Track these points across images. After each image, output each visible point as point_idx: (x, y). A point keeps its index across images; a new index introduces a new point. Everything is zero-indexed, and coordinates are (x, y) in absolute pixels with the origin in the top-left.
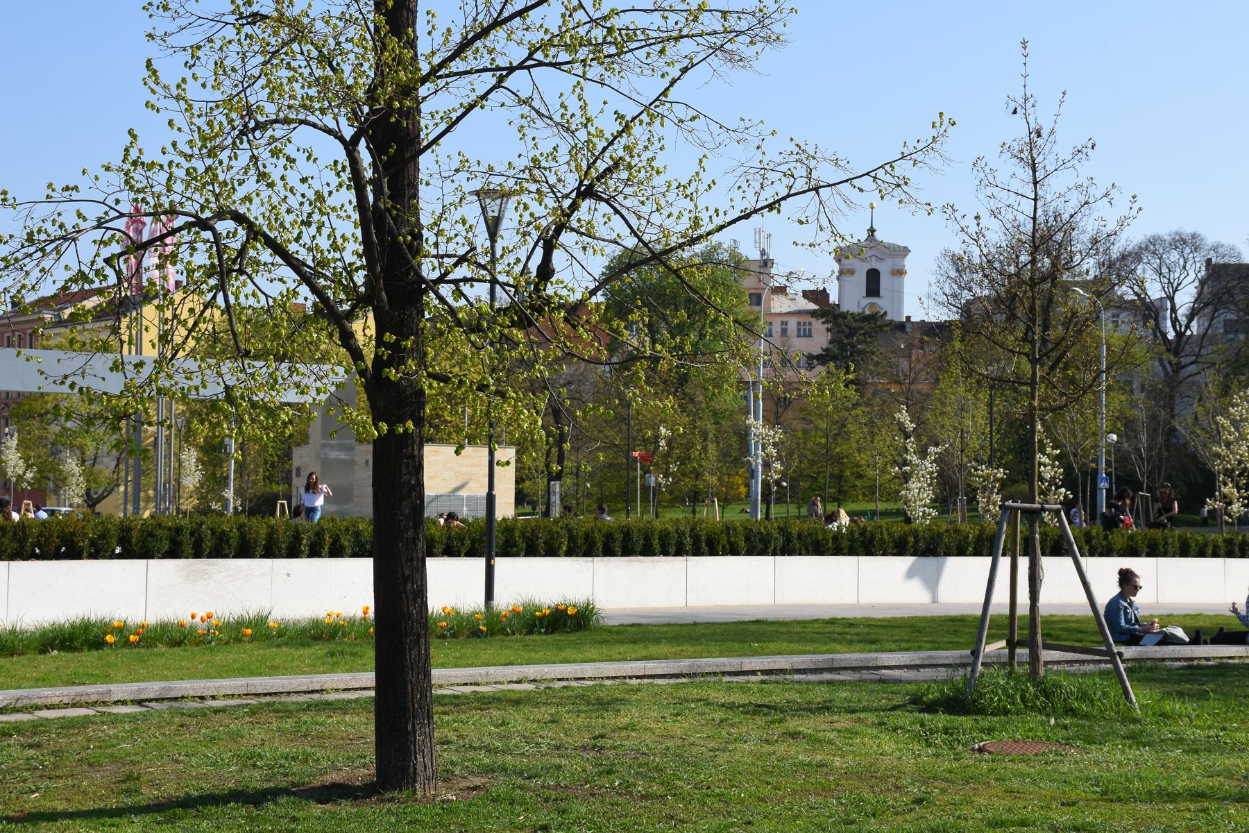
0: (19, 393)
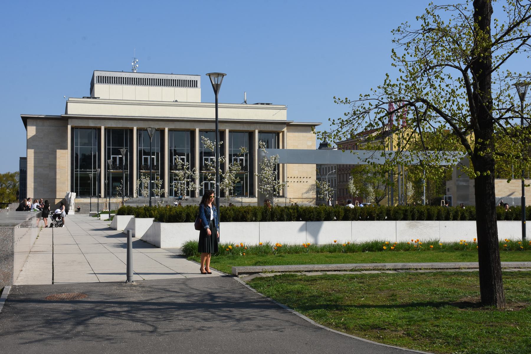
0: (353, 165)
